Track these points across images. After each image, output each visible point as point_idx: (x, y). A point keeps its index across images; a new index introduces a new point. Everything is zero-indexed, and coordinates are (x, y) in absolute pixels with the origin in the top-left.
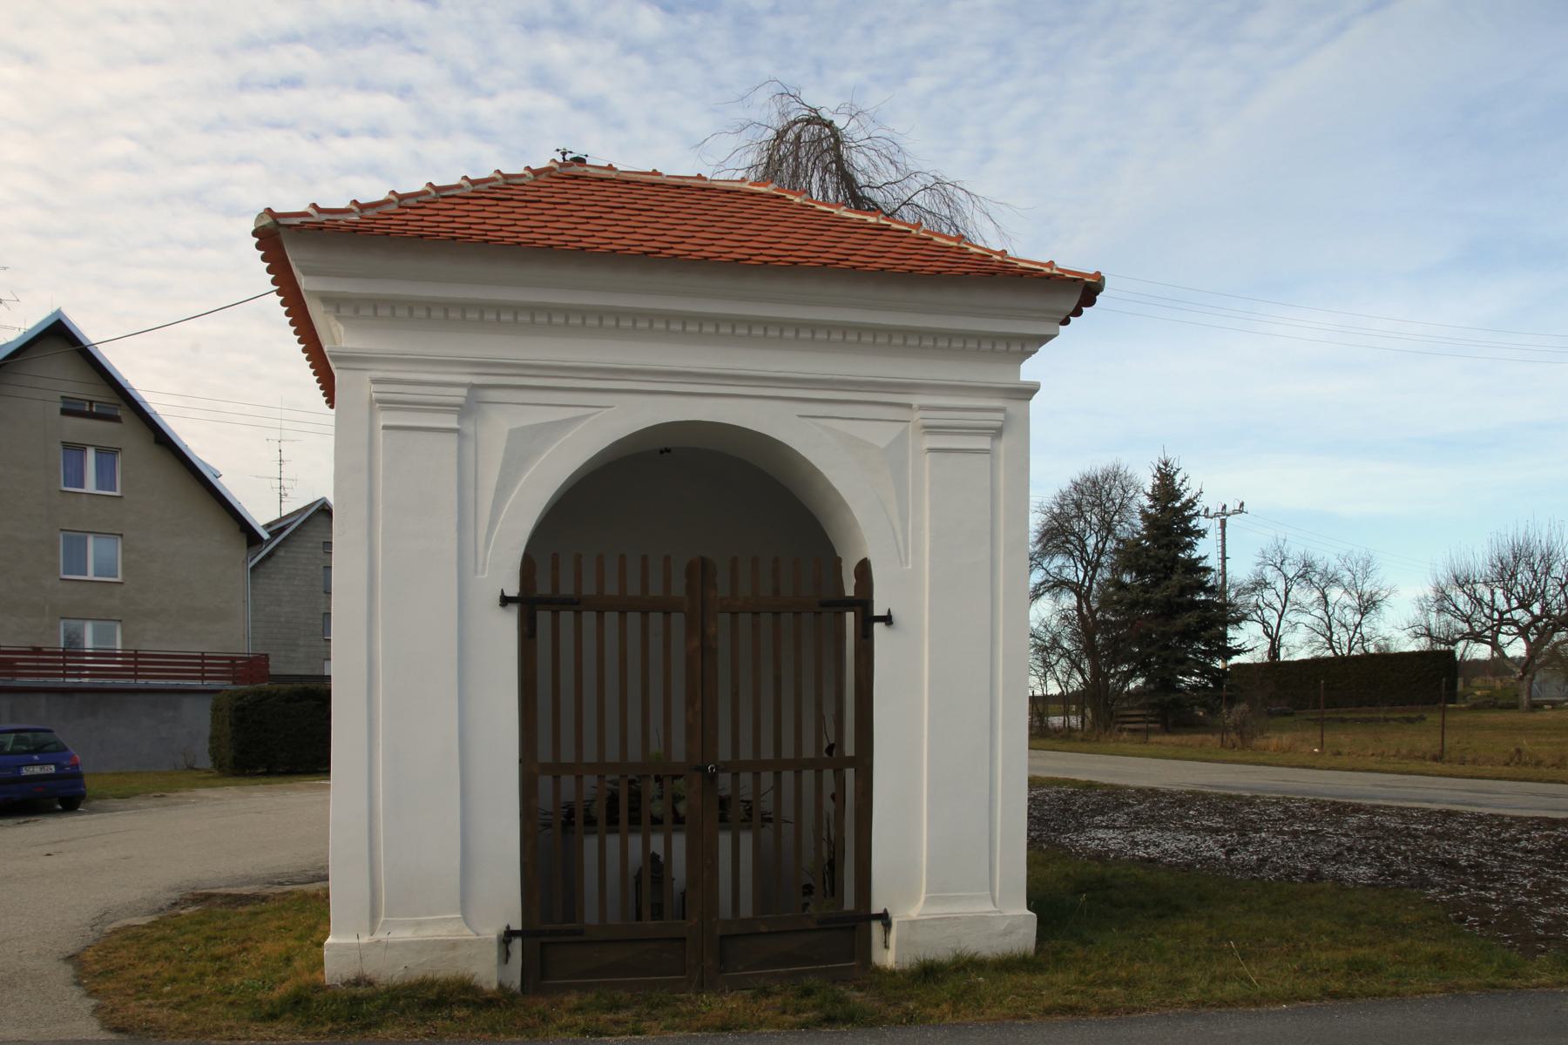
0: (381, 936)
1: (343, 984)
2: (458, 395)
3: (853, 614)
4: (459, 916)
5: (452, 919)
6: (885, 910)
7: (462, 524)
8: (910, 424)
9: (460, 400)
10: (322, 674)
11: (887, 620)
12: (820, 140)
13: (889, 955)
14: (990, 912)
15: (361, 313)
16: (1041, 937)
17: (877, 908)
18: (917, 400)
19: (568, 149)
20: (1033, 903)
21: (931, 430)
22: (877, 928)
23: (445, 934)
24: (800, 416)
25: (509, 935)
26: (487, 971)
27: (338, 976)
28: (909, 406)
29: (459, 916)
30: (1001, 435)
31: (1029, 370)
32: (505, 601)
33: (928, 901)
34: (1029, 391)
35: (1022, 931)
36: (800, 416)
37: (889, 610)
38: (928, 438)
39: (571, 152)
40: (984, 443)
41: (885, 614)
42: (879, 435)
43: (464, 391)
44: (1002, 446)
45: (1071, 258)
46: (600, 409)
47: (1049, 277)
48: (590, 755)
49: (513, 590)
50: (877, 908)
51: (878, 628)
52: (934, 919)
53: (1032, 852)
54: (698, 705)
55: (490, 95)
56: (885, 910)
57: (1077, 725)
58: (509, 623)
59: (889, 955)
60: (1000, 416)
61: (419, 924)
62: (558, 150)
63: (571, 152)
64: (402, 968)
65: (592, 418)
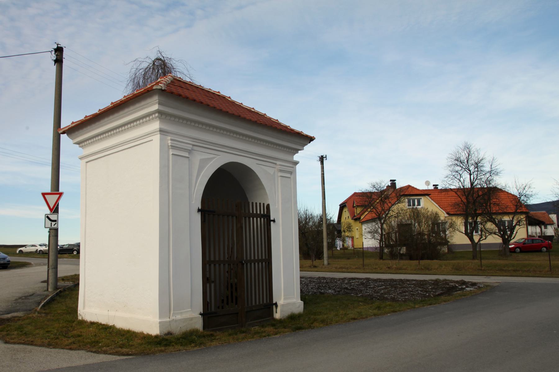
0: (172, 318)
1: (164, 335)
4: (191, 310)
5: (189, 311)
6: (276, 302)
8: (276, 169)
10: (379, 248)
11: (274, 221)
13: (278, 315)
15: (167, 118)
16: (305, 308)
17: (274, 302)
18: (278, 163)
19: (59, 43)
20: (303, 298)
21: (281, 171)
22: (274, 307)
23: (188, 315)
27: (163, 332)
28: (276, 164)
29: (191, 310)
31: (296, 157)
33: (285, 299)
34: (296, 163)
37: (274, 219)
38: (279, 173)
39: (60, 45)
41: (273, 219)
42: (271, 171)
44: (292, 177)
45: (307, 132)
46: (216, 156)
48: (217, 259)
50: (274, 302)
51: (272, 223)
53: (78, 282)
56: (276, 302)
59: (278, 315)
61: (181, 313)
62: (56, 43)
63: (60, 45)
64: (179, 328)
65: (216, 158)
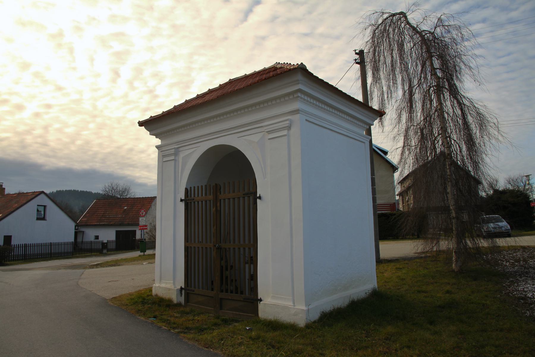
2: (173, 151)
3: (257, 196)
7: (175, 183)
9: (173, 152)
12: (400, 19)
14: (290, 305)
21: (269, 132)
24: (238, 137)
25: (181, 288)
26: (175, 298)
30: (291, 129)
32: (182, 200)
35: (301, 315)
36: (238, 137)
40: (285, 132)
42: (256, 138)
43: (173, 150)
47: (290, 70)
49: (183, 198)
51: (258, 200)
52: (271, 304)
54: (215, 227)
55: (516, 9)
57: (480, 240)
58: (182, 206)
60: (288, 122)
